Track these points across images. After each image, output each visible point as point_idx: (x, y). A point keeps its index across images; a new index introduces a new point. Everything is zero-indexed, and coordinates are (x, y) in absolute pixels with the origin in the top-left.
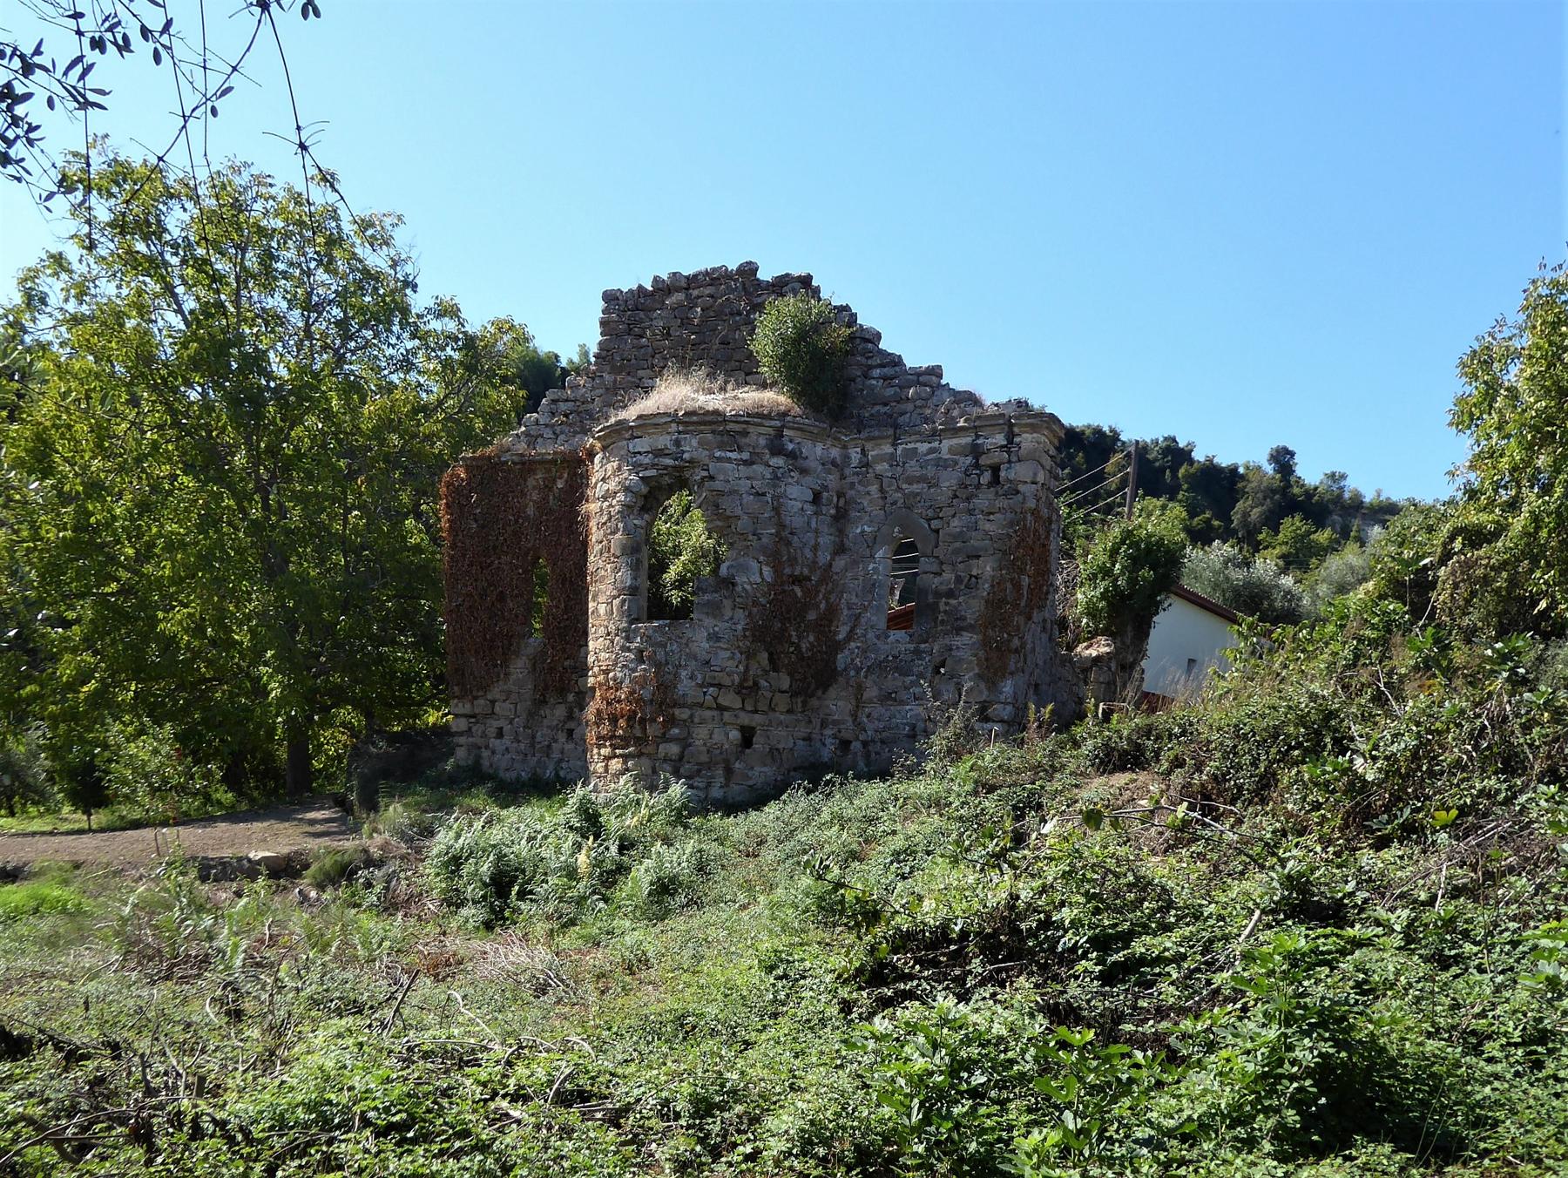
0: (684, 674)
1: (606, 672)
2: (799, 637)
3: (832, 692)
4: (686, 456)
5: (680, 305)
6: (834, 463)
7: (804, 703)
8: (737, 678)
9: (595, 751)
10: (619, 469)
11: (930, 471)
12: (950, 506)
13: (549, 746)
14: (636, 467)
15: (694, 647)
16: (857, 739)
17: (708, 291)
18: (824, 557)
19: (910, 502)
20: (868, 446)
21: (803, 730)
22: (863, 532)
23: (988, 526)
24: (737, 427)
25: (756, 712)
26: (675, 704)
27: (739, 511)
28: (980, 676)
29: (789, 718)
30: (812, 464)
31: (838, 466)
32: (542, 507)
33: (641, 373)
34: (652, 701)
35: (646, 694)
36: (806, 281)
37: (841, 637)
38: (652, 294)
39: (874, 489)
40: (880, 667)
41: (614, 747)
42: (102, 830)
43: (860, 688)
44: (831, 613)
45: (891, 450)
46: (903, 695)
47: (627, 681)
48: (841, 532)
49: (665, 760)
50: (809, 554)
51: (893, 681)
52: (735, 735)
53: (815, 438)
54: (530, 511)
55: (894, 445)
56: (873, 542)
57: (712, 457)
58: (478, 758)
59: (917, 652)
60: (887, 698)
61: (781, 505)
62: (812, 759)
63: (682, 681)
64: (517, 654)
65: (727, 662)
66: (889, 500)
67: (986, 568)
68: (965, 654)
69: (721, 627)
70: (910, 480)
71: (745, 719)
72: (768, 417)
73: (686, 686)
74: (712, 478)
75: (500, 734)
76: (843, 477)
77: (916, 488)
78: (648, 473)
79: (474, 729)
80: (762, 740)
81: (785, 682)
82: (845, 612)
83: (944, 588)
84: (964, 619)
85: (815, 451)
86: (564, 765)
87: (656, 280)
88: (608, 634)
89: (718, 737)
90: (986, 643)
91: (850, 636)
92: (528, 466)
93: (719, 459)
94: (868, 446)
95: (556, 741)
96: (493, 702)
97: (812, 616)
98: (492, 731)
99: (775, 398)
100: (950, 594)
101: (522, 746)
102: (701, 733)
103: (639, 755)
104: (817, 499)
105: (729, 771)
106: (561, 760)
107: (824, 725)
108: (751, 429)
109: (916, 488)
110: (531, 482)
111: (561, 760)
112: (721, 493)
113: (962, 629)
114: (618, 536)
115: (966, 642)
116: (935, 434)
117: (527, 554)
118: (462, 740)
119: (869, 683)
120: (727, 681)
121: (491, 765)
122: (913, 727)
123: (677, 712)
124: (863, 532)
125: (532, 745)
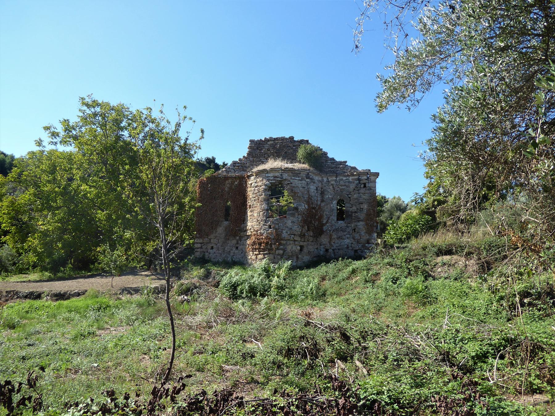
0: (284, 231)
1: (257, 231)
2: (315, 222)
3: (323, 236)
4: (284, 178)
5: (273, 144)
6: (320, 181)
7: (316, 239)
8: (299, 233)
9: (251, 253)
10: (262, 180)
11: (347, 184)
12: (353, 192)
13: (230, 252)
14: (268, 180)
15: (287, 225)
16: (331, 249)
17: (281, 141)
18: (319, 203)
19: (342, 190)
20: (329, 177)
21: (316, 247)
22: (329, 197)
23: (364, 197)
24: (298, 172)
25: (304, 241)
26: (282, 240)
27: (299, 191)
28: (366, 232)
29: (313, 243)
30: (316, 181)
31: (321, 181)
32: (230, 188)
33: (261, 158)
34: (274, 239)
35: (272, 237)
36: (307, 141)
37: (324, 222)
38: (264, 141)
39: (331, 187)
40: (337, 230)
41: (259, 251)
42: (48, 281)
43: (331, 235)
44: (321, 217)
45: (335, 179)
46: (344, 237)
47: (265, 233)
48: (322, 197)
49: (278, 255)
50: (316, 202)
51: (340, 234)
52: (299, 248)
53: (316, 175)
54: (226, 189)
55: (336, 177)
56: (332, 199)
57: (291, 179)
58: (204, 256)
59: (347, 226)
60: (339, 238)
61: (309, 190)
62: (318, 254)
63: (283, 233)
64: (220, 226)
65: (297, 229)
66: (336, 190)
67: (365, 206)
68: (361, 227)
69: (295, 219)
70: (341, 186)
71: (302, 244)
72: (306, 170)
73: (285, 235)
74: (291, 183)
75: (212, 248)
76: (322, 184)
77: (343, 187)
78: (272, 182)
79: (203, 247)
80: (306, 249)
81: (311, 234)
82: (325, 216)
83: (353, 211)
84: (360, 218)
85: (317, 178)
86: (234, 257)
87: (265, 138)
88: (258, 221)
89: (294, 248)
90: (367, 224)
91: (327, 222)
92: (226, 178)
93: (293, 179)
94: (329, 177)
95: (232, 250)
96: (210, 239)
97: (317, 217)
98: (209, 247)
99: (306, 166)
100: (355, 212)
101: (220, 252)
102: (289, 248)
103: (269, 253)
104: (317, 189)
105: (297, 258)
106: (233, 256)
107: (321, 245)
108: (302, 173)
109: (343, 187)
110: (227, 182)
111: (233, 256)
112: (294, 187)
113: (360, 221)
114: (263, 196)
115: (361, 224)
116: (348, 176)
117: (225, 200)
118: (199, 250)
119: (333, 234)
120: (297, 234)
121: (208, 257)
122: (348, 245)
123: (282, 242)
124: (329, 197)
125: (224, 251)
